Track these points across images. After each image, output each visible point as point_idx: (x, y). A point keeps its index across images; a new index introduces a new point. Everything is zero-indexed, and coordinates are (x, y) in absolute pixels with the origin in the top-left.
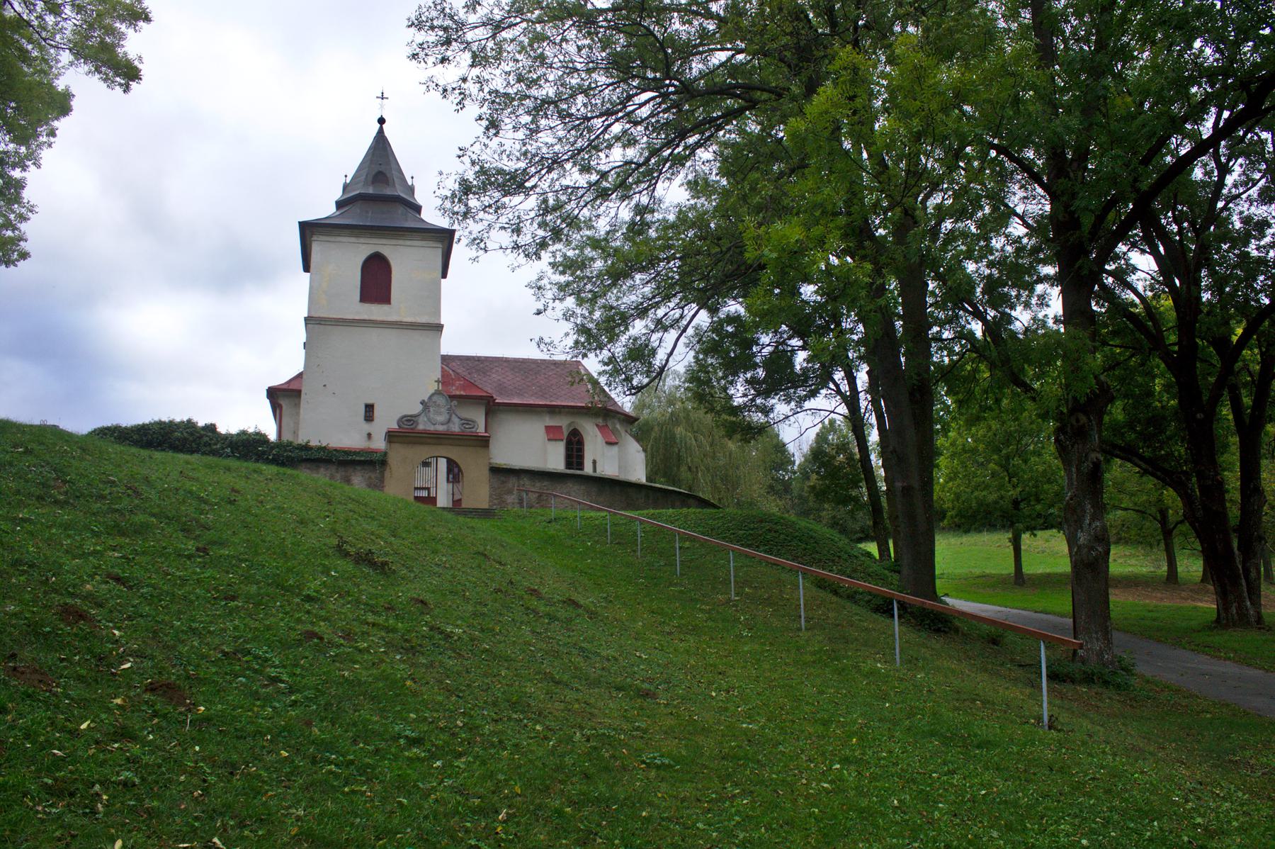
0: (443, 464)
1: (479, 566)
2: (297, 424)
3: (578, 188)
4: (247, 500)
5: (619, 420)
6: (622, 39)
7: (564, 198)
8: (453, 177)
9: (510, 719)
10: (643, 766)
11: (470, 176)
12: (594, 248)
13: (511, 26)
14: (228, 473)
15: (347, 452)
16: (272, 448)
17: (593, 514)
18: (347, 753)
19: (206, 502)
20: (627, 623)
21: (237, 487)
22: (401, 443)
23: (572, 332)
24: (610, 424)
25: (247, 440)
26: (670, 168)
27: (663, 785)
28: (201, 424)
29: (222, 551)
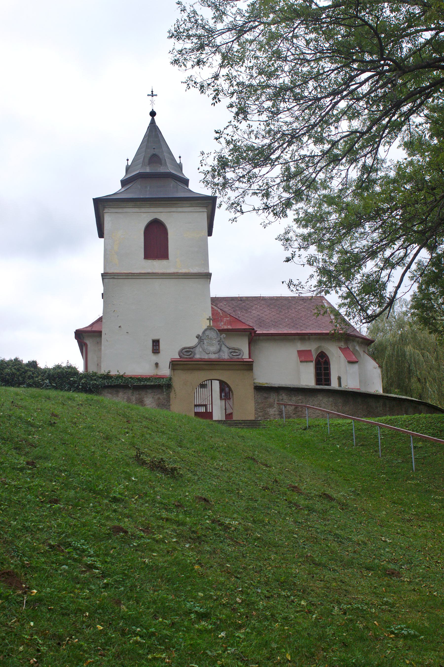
0: (216, 385)
1: (250, 469)
2: (99, 358)
3: (314, 156)
4: (64, 422)
5: (358, 342)
6: (343, 30)
7: (303, 165)
8: (213, 155)
9: (279, 596)
10: (392, 636)
11: (226, 153)
12: (330, 204)
13: (252, 28)
14: (48, 401)
15: (140, 379)
16: (81, 378)
17: (340, 421)
18: (150, 626)
19: (32, 425)
20: (373, 513)
21: (56, 412)
22: (183, 370)
23: (316, 274)
24: (350, 346)
25: (62, 372)
26: (389, 133)
27: (411, 653)
28: (25, 361)
29: (46, 464)
